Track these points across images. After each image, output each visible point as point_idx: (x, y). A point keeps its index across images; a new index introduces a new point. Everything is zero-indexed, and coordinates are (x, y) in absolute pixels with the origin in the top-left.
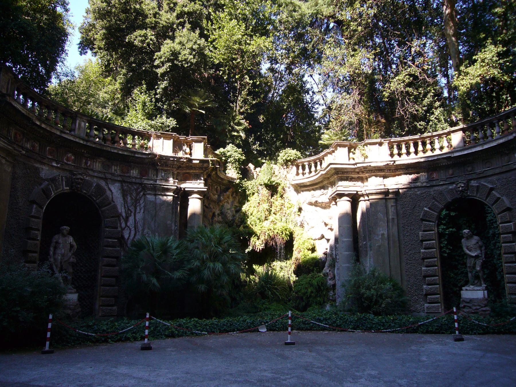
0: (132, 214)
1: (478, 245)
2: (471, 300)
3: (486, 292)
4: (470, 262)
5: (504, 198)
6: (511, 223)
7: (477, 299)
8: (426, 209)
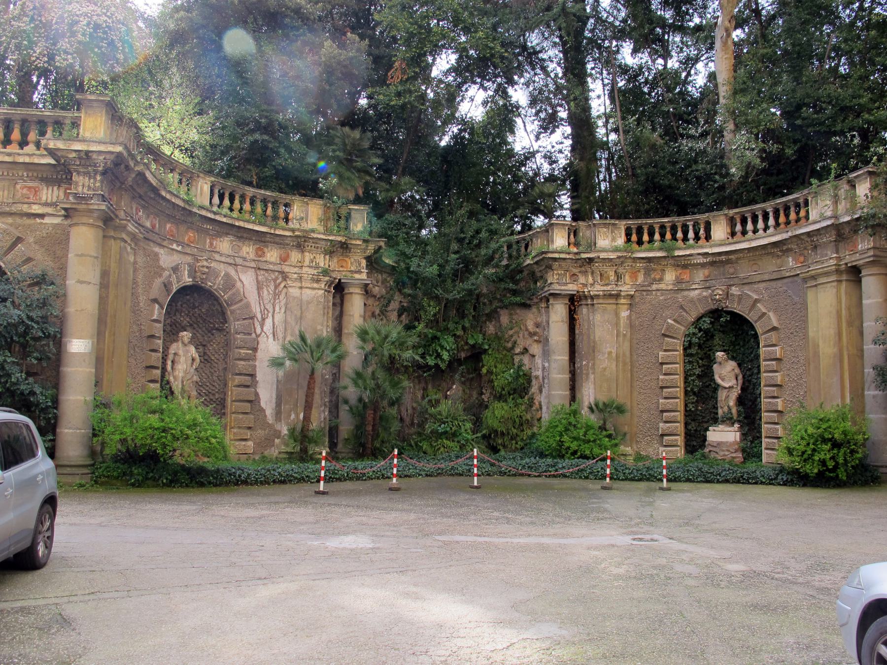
0: (270, 315)
2: (719, 444)
3: (738, 434)
4: (722, 395)
5: (771, 314)
8: (669, 321)
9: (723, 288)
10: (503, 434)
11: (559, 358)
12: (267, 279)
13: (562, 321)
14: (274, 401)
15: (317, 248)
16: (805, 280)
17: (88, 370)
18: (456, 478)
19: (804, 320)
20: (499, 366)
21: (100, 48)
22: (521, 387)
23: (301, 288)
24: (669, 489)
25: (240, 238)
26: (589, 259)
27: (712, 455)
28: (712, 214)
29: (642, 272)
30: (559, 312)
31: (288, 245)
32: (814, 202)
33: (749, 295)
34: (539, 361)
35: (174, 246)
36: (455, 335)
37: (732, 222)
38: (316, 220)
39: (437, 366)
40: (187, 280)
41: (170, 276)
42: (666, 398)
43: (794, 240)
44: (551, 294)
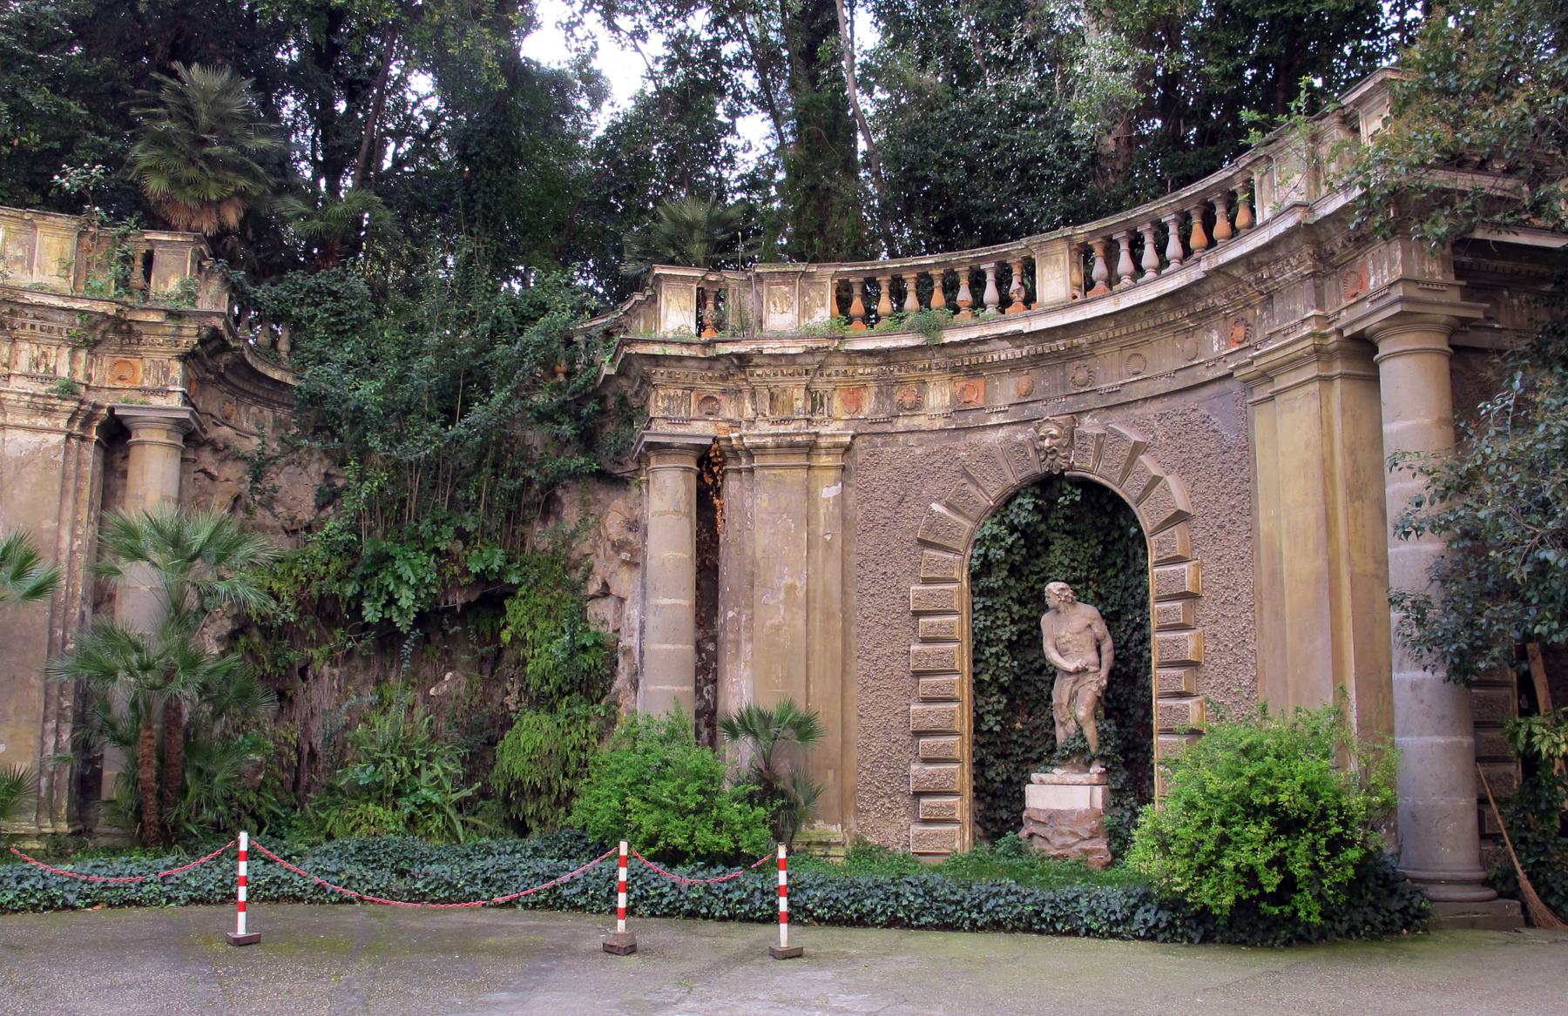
1: (1089, 633)
2: (1054, 816)
3: (1099, 790)
4: (1061, 690)
5: (1172, 481)
6: (1185, 566)
7: (1072, 812)
8: (935, 507)
9: (1060, 419)
10: (536, 792)
11: (666, 601)
13: (676, 512)
15: (50, 330)
16: (1249, 384)
18: (286, 907)
19: (1247, 494)
20: (541, 625)
22: (591, 677)
24: (794, 954)
26: (740, 356)
27: (1037, 844)
28: (1036, 238)
29: (873, 389)
30: (666, 494)
32: (1266, 186)
33: (1119, 435)
34: (633, 612)
36: (437, 551)
37: (1084, 254)
38: (54, 267)
42: (926, 700)
43: (1219, 282)
44: (651, 446)
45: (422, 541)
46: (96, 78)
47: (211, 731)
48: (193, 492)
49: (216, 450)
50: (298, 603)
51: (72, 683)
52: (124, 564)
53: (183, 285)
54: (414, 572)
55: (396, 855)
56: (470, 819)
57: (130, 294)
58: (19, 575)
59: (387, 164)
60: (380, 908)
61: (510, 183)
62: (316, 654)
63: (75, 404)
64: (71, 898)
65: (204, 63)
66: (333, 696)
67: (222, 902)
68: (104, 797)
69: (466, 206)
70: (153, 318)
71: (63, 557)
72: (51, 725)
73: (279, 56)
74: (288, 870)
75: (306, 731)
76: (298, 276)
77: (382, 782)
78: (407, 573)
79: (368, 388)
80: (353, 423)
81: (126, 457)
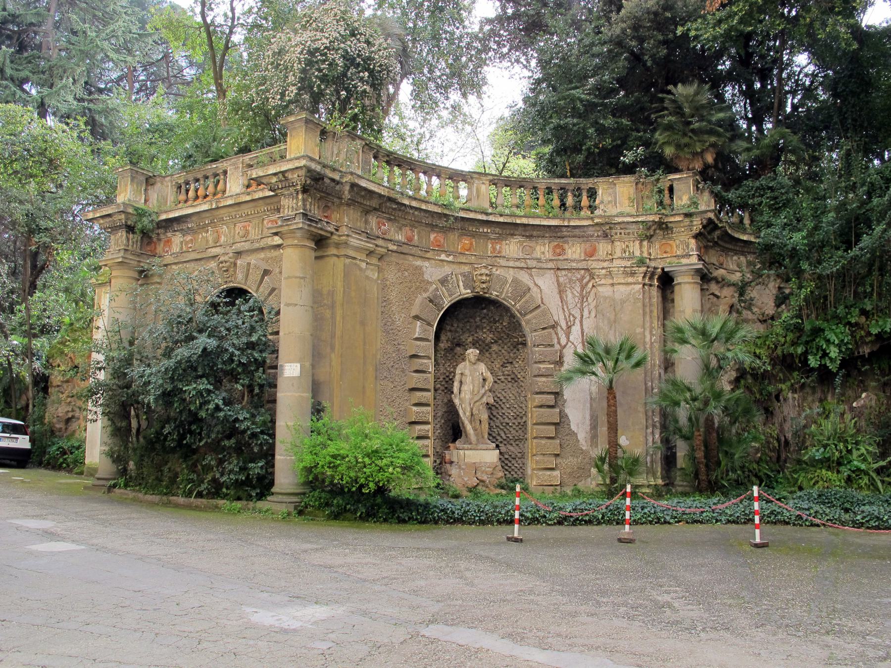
0: (577, 321)
12: (570, 280)
14: (588, 422)
15: (629, 234)
17: (297, 395)
18: (782, 527)
21: (320, 70)
23: (612, 285)
25: (530, 237)
31: (592, 236)
35: (443, 257)
36: (849, 323)
38: (627, 202)
39: (823, 368)
40: (467, 293)
41: (437, 290)
45: (840, 319)
46: (632, 105)
47: (730, 431)
48: (708, 306)
49: (718, 282)
50: (771, 360)
51: (658, 409)
52: (677, 346)
53: (690, 199)
54: (837, 336)
55: (842, 500)
56: (886, 479)
57: (664, 208)
58: (629, 357)
59: (789, 109)
60: (836, 531)
61: (867, 102)
62: (784, 387)
63: (645, 269)
64: (668, 518)
65: (684, 83)
66: (795, 409)
67: (745, 523)
68: (679, 466)
69: (841, 121)
70: (678, 219)
71: (648, 346)
72: (650, 430)
73: (720, 67)
74: (780, 507)
75: (782, 430)
76: (749, 183)
77: (829, 458)
78: (833, 337)
79: (797, 237)
80: (792, 257)
81: (673, 292)
